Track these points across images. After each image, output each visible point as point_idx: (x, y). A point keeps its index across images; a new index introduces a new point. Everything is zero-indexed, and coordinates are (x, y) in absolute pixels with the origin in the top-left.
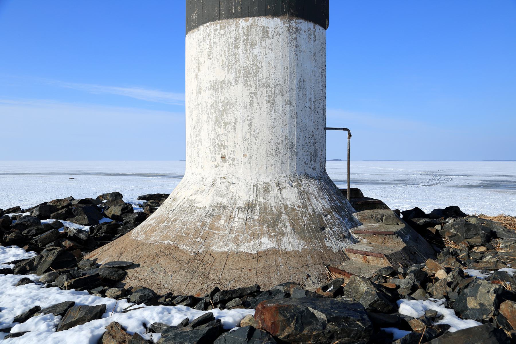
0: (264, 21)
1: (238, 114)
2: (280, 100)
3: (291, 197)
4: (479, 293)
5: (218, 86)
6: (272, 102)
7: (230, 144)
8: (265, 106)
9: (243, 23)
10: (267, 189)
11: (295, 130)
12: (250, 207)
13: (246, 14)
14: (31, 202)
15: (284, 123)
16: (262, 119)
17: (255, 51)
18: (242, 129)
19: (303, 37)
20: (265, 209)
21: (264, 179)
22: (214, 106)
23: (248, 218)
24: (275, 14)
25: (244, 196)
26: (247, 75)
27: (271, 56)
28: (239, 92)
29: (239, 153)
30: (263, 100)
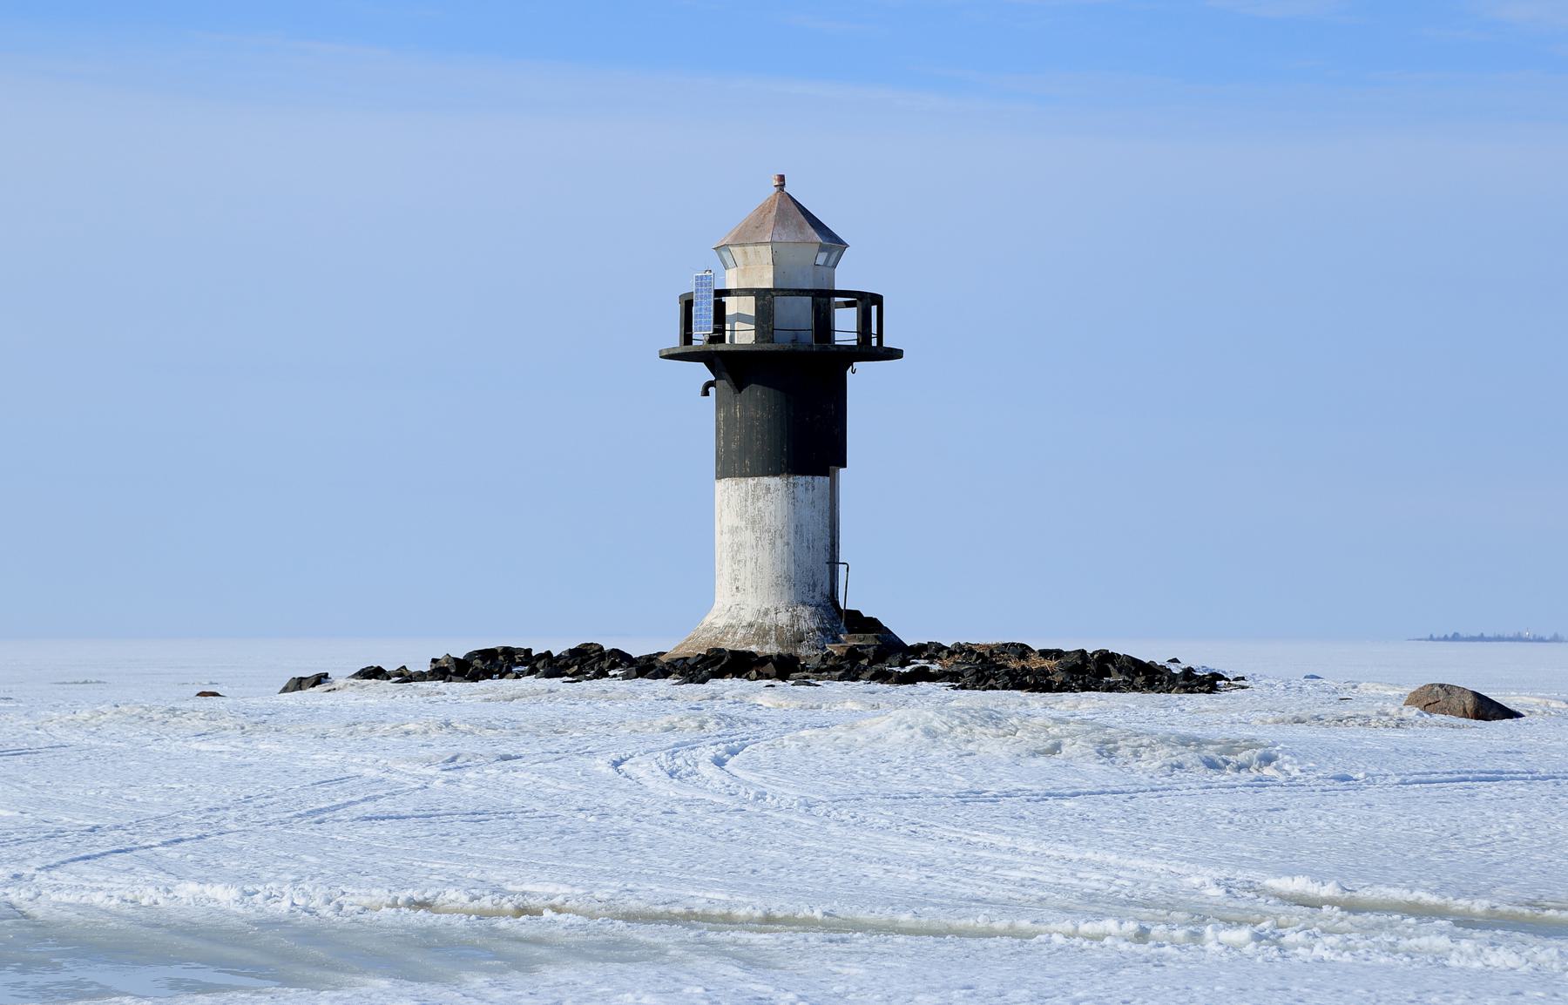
0: (766, 480)
1: (747, 553)
2: (779, 542)
3: (784, 618)
4: (754, 648)
5: (734, 530)
6: (773, 544)
7: (742, 577)
8: (767, 547)
9: (751, 481)
10: (766, 613)
11: (793, 567)
12: (751, 625)
13: (754, 474)
14: (386, 701)
15: (783, 561)
16: (765, 557)
17: (760, 504)
18: (750, 565)
19: (800, 490)
20: (761, 626)
21: (766, 606)
22: (731, 546)
23: (1281, 778)
24: (775, 474)
25: (748, 617)
26: (754, 522)
27: (772, 507)
28: (748, 537)
29: (748, 584)
30: (766, 542)
